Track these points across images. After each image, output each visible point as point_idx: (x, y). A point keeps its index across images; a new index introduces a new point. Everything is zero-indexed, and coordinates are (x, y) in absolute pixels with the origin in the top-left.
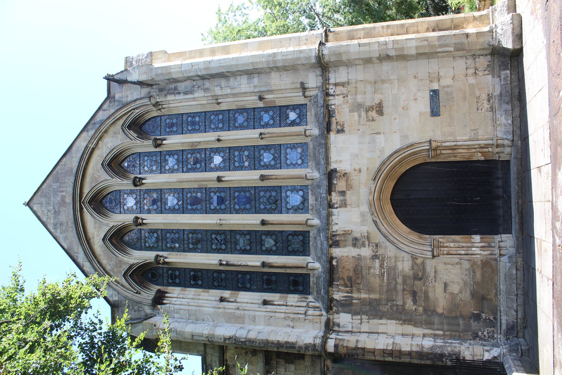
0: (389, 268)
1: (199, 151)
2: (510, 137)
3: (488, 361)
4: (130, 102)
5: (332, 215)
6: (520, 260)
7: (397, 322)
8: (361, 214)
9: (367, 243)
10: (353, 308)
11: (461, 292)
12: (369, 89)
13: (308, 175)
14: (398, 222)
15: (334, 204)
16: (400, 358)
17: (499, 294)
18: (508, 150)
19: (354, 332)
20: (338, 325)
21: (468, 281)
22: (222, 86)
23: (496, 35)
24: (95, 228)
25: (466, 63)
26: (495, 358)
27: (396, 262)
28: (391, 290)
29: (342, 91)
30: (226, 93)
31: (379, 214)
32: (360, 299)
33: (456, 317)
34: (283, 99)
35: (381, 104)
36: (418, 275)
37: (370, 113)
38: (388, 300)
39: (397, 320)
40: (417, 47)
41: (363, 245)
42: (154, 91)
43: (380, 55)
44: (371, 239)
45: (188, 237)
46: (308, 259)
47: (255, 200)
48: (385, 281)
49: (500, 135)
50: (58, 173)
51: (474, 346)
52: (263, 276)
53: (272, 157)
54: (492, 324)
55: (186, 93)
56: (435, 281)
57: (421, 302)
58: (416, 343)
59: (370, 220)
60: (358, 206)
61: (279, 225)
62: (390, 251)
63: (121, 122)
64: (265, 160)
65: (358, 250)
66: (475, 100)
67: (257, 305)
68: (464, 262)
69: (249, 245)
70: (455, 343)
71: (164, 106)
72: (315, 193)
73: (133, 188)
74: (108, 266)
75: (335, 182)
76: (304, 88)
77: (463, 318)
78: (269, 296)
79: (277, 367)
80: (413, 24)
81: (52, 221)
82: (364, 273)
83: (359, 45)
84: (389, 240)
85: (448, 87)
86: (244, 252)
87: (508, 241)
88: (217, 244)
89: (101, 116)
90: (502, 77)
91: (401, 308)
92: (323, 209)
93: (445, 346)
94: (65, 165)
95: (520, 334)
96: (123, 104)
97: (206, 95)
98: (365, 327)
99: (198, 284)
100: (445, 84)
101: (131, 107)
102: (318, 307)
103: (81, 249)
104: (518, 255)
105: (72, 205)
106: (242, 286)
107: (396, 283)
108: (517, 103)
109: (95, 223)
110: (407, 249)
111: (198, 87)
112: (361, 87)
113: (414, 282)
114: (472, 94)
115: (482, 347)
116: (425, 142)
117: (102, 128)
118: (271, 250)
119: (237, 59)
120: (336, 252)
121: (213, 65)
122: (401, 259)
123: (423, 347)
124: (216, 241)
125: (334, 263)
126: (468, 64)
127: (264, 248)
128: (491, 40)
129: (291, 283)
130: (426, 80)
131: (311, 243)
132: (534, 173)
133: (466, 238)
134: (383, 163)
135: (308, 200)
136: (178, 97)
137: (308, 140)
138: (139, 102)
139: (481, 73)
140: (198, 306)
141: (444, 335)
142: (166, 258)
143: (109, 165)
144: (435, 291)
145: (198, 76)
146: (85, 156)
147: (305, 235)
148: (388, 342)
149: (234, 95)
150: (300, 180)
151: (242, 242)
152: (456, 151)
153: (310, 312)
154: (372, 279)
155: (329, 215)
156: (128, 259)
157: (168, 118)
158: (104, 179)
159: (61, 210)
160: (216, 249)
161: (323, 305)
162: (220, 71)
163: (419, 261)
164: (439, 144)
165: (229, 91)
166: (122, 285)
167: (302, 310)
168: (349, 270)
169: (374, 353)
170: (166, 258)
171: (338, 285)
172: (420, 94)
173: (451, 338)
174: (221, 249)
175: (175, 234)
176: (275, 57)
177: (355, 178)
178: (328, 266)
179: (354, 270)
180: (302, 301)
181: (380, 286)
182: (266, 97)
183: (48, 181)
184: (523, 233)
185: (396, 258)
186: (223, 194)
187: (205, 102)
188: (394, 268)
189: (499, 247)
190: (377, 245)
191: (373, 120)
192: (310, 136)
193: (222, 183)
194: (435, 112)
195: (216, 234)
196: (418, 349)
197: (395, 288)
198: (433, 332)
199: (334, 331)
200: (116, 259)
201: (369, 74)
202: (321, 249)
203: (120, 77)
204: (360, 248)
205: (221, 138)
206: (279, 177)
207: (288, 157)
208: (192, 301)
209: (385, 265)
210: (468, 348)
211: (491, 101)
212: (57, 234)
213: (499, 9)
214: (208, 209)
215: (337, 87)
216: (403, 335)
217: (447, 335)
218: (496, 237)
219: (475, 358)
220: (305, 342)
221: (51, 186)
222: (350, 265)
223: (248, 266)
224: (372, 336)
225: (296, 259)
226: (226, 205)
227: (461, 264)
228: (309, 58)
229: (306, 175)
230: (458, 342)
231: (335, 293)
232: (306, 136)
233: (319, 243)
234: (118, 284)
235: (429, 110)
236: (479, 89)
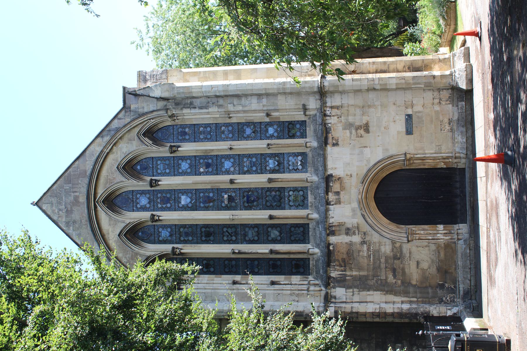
0: (374, 251)
1: (211, 157)
2: (465, 152)
4: (147, 113)
5: (329, 210)
6: (472, 242)
7: (382, 292)
8: (352, 210)
9: (357, 232)
10: (347, 283)
11: (429, 268)
12: (358, 112)
13: (309, 178)
14: (381, 215)
15: (330, 202)
16: (385, 318)
17: (457, 269)
18: (463, 161)
19: (348, 303)
21: (435, 259)
22: (235, 104)
23: (455, 78)
24: (110, 225)
25: (433, 95)
26: (455, 314)
27: (379, 246)
28: (376, 268)
29: (336, 112)
30: (238, 110)
31: (366, 209)
32: (351, 276)
33: (426, 287)
34: (287, 116)
35: (367, 124)
37: (359, 131)
38: (374, 276)
40: (397, 84)
41: (354, 233)
42: (170, 105)
43: (368, 88)
44: (360, 228)
45: (201, 231)
46: (308, 246)
48: (372, 261)
49: (457, 150)
50: (70, 175)
52: (269, 261)
55: (201, 108)
56: (410, 260)
58: (397, 307)
59: (359, 214)
60: (350, 203)
61: (284, 219)
62: (375, 238)
63: (137, 130)
64: (271, 166)
65: (350, 237)
66: (439, 123)
67: (266, 286)
68: (432, 244)
69: (257, 236)
71: (178, 118)
72: (314, 193)
73: (149, 188)
74: (124, 258)
75: (331, 185)
76: (305, 108)
77: (432, 287)
78: (275, 278)
80: (393, 62)
81: (64, 220)
82: (355, 255)
83: (353, 80)
84: (374, 230)
85: (419, 112)
86: (252, 242)
87: (464, 229)
89: (116, 124)
92: (321, 206)
93: (419, 308)
94: (78, 167)
95: (473, 297)
96: (139, 115)
97: (219, 110)
98: (356, 298)
99: (210, 271)
100: (417, 110)
102: (317, 285)
104: (470, 239)
105: (86, 204)
107: (380, 262)
108: (469, 126)
109: (109, 220)
110: (388, 236)
111: (213, 103)
112: (352, 110)
113: (394, 261)
114: (437, 119)
116: (402, 154)
117: (118, 135)
119: (252, 84)
120: (333, 239)
121: (230, 88)
122: (384, 243)
123: (402, 309)
124: (227, 234)
125: (331, 248)
126: (435, 95)
127: (270, 238)
128: (451, 81)
130: (402, 106)
131: (310, 233)
132: (479, 180)
133: (433, 227)
134: (369, 170)
135: (308, 198)
136: (193, 111)
137: (307, 150)
138: (155, 113)
140: (214, 289)
141: (417, 301)
142: (181, 249)
143: (124, 168)
146: (100, 160)
147: (305, 227)
149: (245, 112)
150: (302, 182)
151: (251, 234)
152: (425, 161)
153: (312, 288)
154: (361, 260)
155: (327, 210)
156: (144, 252)
157: (180, 127)
158: (119, 181)
159: (73, 209)
160: (228, 240)
161: (322, 282)
162: (236, 93)
163: (398, 245)
165: (240, 108)
167: (305, 287)
168: (343, 253)
169: (365, 315)
170: (181, 249)
171: (334, 265)
172: (397, 117)
173: (423, 303)
174: (231, 240)
175: (188, 229)
176: (284, 85)
177: (347, 181)
178: (326, 250)
179: (347, 253)
180: (303, 280)
181: (368, 265)
182: (273, 114)
183: (58, 182)
184: (474, 222)
185: (380, 243)
187: (218, 116)
188: (379, 251)
189: (457, 234)
191: (361, 137)
192: (310, 147)
193: (234, 185)
194: (409, 132)
195: (228, 228)
196: (399, 311)
197: (380, 266)
198: (409, 299)
199: (332, 302)
201: (359, 100)
202: (320, 237)
203: (142, 93)
204: (352, 236)
205: (233, 147)
206: (284, 180)
208: (207, 285)
209: (372, 248)
210: (436, 308)
211: (451, 124)
212: (70, 232)
213: (457, 55)
214: (177, 207)
215: (333, 109)
217: (420, 301)
218: (455, 226)
219: (441, 315)
221: (63, 187)
222: (344, 250)
223: (257, 253)
224: (362, 304)
225: (298, 246)
226: (236, 203)
227: (429, 247)
228: (313, 87)
229: (307, 179)
231: (332, 272)
232: (307, 147)
233: (318, 232)
235: (404, 130)
236: (442, 114)
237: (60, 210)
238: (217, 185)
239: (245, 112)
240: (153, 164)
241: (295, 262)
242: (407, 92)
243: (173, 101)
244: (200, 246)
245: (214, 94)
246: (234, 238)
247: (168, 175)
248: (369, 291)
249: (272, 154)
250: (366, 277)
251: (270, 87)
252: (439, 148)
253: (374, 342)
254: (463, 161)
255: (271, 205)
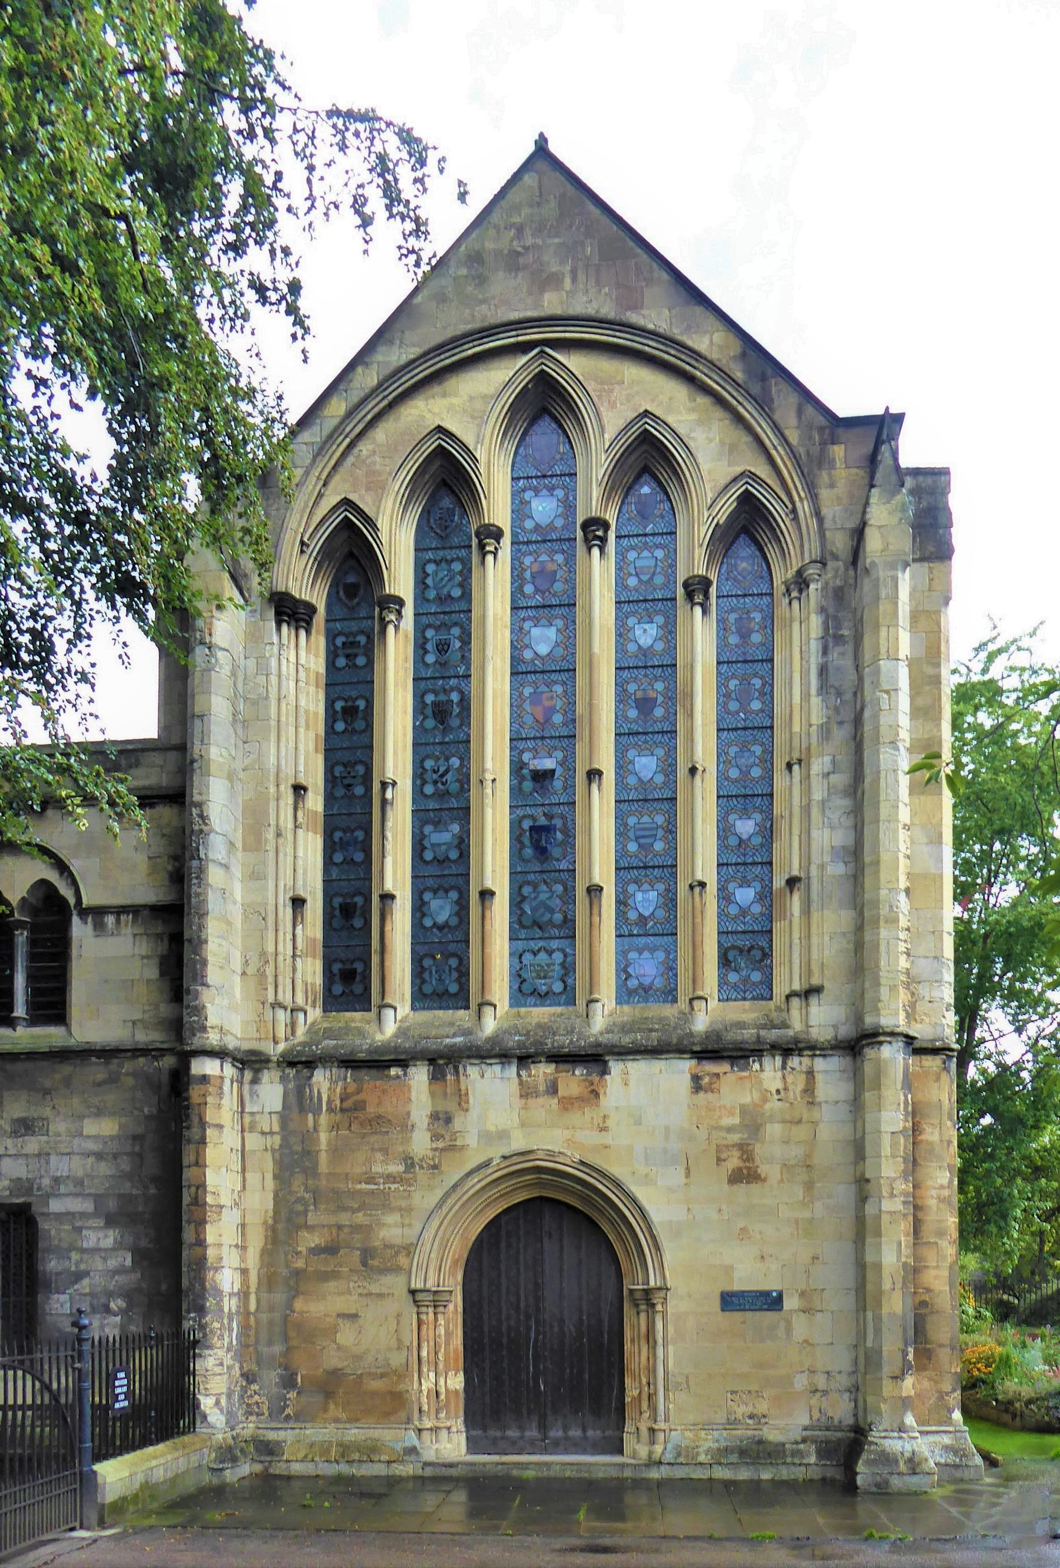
3: (196, 1405)
4: (814, 497)
7: (271, 1213)
9: (440, 1144)
10: (295, 1115)
12: (795, 1152)
13: (599, 1005)
20: (255, 1081)
24: (471, 398)
25: (840, 1372)
26: (205, 1417)
27: (400, 1209)
28: (339, 1200)
32: (316, 1129)
33: (286, 1339)
36: (373, 1258)
37: (736, 1153)
38: (316, 1193)
39: (275, 1212)
41: (436, 1137)
45: (452, 689)
47: (542, 872)
48: (358, 1187)
51: (225, 1377)
53: (647, 914)
54: (278, 1412)
55: (823, 671)
56: (360, 1295)
57: (319, 1264)
60: (523, 1125)
62: (425, 1198)
63: (763, 471)
64: (639, 896)
66: (754, 1387)
67: (290, 883)
70: (230, 1336)
71: (795, 604)
74: (370, 447)
76: (811, 992)
79: (147, 935)
81: (490, 245)
82: (373, 1139)
84: (447, 1195)
85: (789, 1330)
87: (449, 1446)
88: (435, 772)
90: (802, 1446)
91: (300, 1220)
97: (814, 728)
101: (801, 499)
102: (293, 1033)
103: (413, 352)
106: (336, 839)
107: (354, 1211)
109: (484, 397)
110: (429, 1235)
112: (801, 1132)
115: (224, 1390)
116: (664, 1277)
118: (424, 915)
119: (894, 818)
120: (419, 1075)
122: (407, 1222)
123: (216, 1269)
124: (442, 769)
125: (393, 1071)
126: (838, 1377)
129: (348, 966)
134: (618, 1184)
136: (815, 646)
137: (682, 1004)
139: (814, 1401)
141: (248, 1313)
142: (397, 628)
144: (340, 1294)
145: (862, 709)
146: (673, 352)
148: (222, 1193)
149: (806, 809)
152: (643, 1342)
158: (605, 420)
159: (520, 275)
161: (300, 1044)
162: (867, 771)
163: (403, 1261)
164: (659, 1308)
165: (817, 795)
166: (320, 495)
167: (286, 997)
170: (397, 628)
171: (345, 1079)
172: (774, 1267)
174: (424, 782)
179: (380, 1117)
182: (796, 897)
183: (605, 220)
185: (409, 1210)
186: (558, 784)
187: (796, 728)
188: (386, 1207)
190: (435, 1167)
191: (719, 1160)
192: (692, 1009)
194: (730, 1301)
197: (345, 1209)
198: (253, 1289)
200: (390, 474)
204: (429, 1130)
205: (698, 778)
206: (595, 933)
207: (646, 954)
209: (393, 1186)
210: (221, 1364)
211: (750, 1422)
216: (243, 1226)
218: (461, 1421)
220: (208, 1005)
222: (388, 1108)
223: (383, 857)
227: (399, 1348)
228: (877, 1011)
230: (234, 1342)
232: (691, 1000)
234: (321, 483)
235: (737, 1287)
237: (520, 229)
238: (586, 721)
239: (806, 809)
240: (654, 535)
241: (359, 970)
242: (852, 1298)
243: (852, 581)
244: (405, 689)
245: (868, 699)
246: (429, 789)
247: (621, 584)
248: (276, 1177)
249: (674, 901)
250: (311, 1171)
251: (883, 876)
252: (679, 1384)
253: (134, 1192)
254: (643, 1451)
255: (524, 899)
